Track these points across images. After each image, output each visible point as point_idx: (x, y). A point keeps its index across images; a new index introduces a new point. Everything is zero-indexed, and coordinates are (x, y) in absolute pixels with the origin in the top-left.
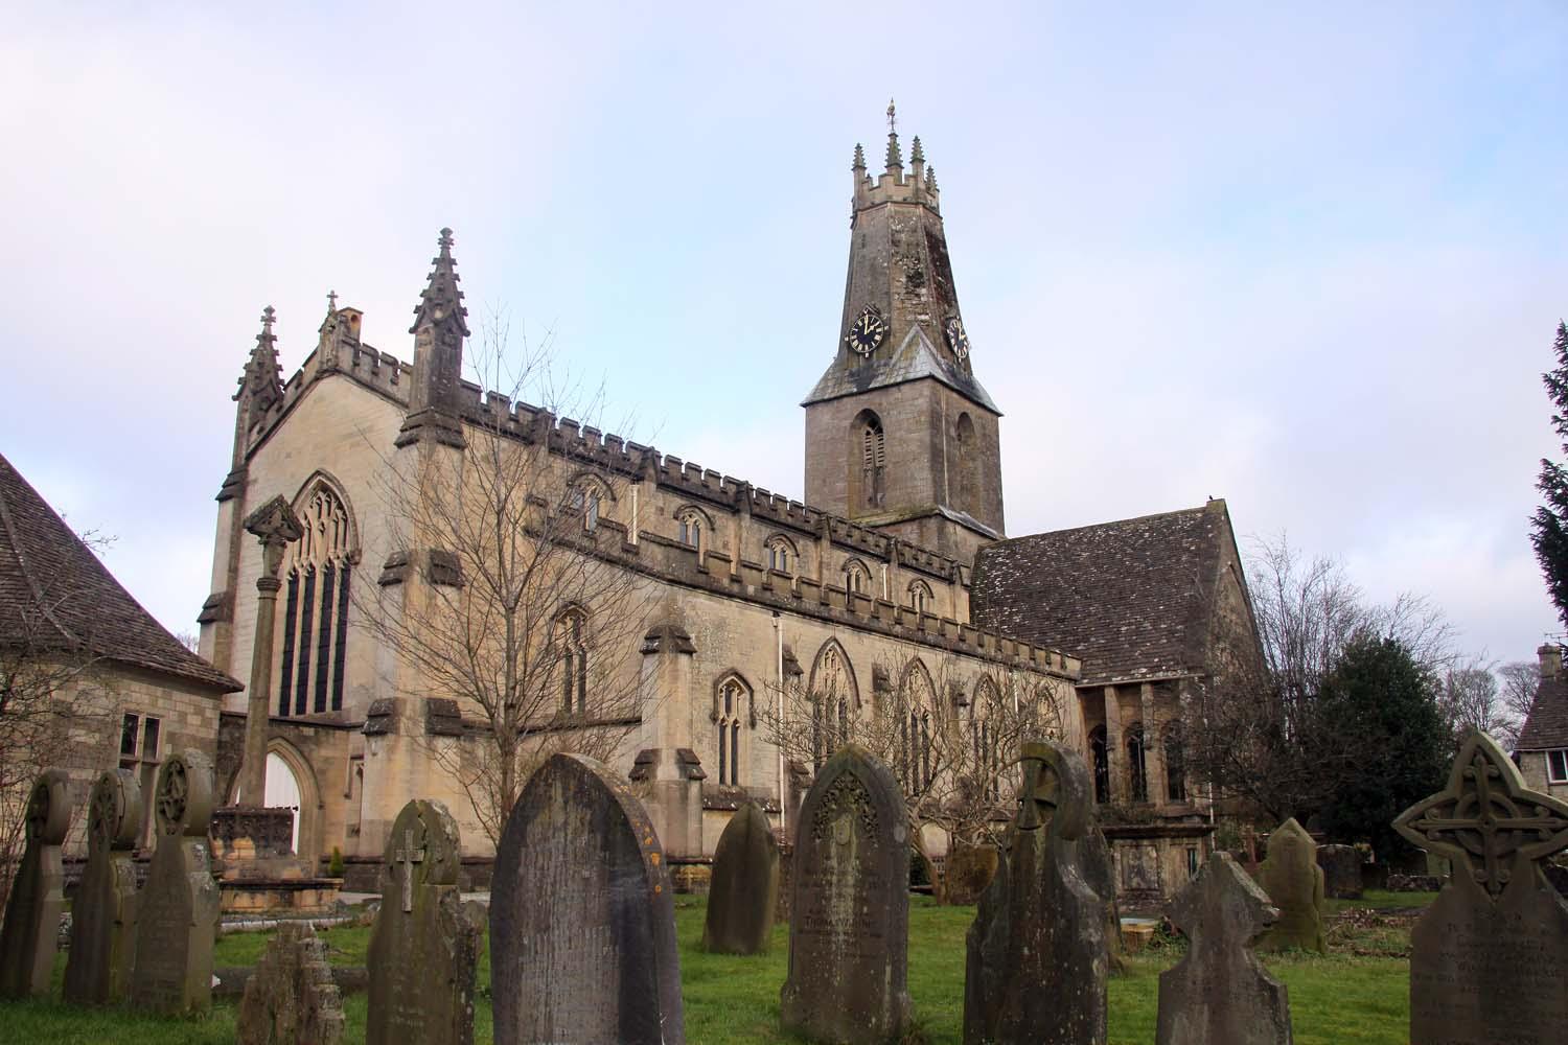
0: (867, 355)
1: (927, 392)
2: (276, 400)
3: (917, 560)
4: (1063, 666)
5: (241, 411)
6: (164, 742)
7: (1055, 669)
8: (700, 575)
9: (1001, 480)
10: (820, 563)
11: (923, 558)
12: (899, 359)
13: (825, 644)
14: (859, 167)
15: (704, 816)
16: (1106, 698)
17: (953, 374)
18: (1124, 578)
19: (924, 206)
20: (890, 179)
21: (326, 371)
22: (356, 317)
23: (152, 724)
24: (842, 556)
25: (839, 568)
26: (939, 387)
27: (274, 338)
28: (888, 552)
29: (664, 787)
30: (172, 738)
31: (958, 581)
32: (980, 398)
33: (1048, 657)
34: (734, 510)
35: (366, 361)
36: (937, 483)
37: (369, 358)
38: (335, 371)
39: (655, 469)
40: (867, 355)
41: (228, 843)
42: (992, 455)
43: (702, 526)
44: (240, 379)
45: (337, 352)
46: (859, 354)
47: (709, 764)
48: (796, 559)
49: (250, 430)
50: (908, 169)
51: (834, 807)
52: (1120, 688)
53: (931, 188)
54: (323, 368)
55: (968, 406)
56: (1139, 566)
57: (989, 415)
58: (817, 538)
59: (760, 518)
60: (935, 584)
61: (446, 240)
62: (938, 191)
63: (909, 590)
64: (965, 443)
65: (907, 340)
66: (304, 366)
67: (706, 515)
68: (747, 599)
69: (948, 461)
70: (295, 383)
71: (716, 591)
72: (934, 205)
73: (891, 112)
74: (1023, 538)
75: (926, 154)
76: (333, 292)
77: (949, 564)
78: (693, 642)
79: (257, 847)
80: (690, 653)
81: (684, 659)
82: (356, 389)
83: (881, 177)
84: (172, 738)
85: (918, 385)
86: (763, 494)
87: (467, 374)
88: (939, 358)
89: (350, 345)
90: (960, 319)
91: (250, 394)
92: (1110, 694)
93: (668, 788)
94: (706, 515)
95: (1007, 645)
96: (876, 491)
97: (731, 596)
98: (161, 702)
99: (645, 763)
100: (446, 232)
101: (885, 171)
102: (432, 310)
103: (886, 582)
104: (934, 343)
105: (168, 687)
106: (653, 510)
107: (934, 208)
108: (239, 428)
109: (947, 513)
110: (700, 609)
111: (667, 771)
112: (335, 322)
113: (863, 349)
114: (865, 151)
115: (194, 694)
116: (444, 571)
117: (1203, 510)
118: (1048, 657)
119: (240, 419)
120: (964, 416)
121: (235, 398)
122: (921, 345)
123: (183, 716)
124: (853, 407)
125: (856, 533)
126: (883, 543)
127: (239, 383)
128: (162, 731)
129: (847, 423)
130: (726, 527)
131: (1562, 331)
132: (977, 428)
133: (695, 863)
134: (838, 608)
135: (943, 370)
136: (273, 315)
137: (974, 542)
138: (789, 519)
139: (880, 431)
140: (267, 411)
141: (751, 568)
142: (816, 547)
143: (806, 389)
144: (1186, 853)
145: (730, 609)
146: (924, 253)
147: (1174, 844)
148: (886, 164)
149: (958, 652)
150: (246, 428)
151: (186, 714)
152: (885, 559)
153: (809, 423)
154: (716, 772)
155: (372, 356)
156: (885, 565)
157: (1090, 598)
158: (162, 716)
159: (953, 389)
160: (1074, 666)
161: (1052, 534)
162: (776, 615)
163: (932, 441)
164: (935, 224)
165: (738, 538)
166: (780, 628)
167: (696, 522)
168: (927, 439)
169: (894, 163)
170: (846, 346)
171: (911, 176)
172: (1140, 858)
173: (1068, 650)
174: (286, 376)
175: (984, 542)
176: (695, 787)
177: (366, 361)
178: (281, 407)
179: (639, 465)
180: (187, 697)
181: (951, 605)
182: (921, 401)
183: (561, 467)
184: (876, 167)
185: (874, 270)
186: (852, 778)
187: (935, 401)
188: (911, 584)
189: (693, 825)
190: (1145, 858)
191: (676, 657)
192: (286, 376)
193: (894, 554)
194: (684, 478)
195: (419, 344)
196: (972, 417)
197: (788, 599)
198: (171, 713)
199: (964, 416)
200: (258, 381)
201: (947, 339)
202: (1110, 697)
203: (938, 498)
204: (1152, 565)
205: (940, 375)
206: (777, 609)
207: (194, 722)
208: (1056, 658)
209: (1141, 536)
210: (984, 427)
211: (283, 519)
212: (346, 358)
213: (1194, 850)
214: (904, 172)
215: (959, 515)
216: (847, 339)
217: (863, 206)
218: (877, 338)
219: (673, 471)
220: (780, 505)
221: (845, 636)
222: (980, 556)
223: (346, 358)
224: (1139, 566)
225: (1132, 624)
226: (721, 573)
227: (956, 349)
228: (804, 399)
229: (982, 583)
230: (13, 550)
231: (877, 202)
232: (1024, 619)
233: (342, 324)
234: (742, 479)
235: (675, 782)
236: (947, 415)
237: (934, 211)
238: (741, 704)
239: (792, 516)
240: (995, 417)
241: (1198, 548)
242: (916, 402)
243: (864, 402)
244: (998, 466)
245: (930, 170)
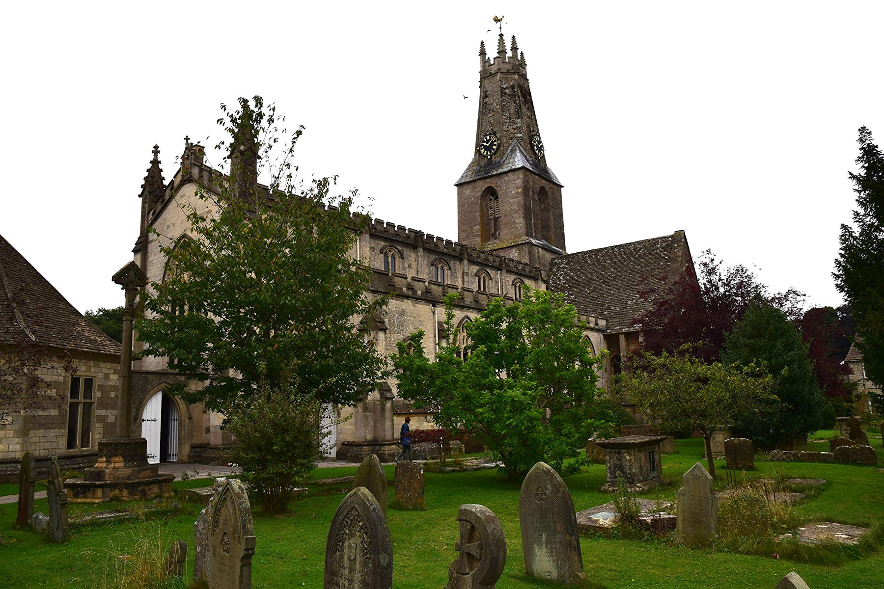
0: (489, 157)
1: (521, 176)
2: (161, 196)
3: (517, 268)
4: (597, 324)
5: (144, 203)
6: (96, 390)
7: (592, 325)
8: (389, 287)
9: (563, 222)
11: (520, 267)
12: (506, 159)
13: (462, 320)
14: (483, 53)
15: (395, 418)
16: (620, 340)
17: (534, 165)
18: (630, 274)
19: (518, 73)
20: (500, 60)
21: (185, 180)
23: (89, 382)
24: (475, 269)
25: (473, 275)
26: (528, 173)
27: (160, 162)
28: (500, 265)
29: (372, 404)
30: (101, 388)
31: (540, 278)
32: (551, 178)
33: (587, 319)
34: (414, 247)
35: (205, 174)
37: (207, 173)
39: (369, 227)
40: (489, 157)
41: (109, 459)
42: (558, 209)
43: (397, 256)
44: (142, 185)
45: (191, 170)
46: (485, 156)
48: (449, 271)
49: (149, 213)
50: (509, 54)
51: (347, 531)
52: (627, 334)
53: (522, 64)
54: (185, 177)
56: (637, 268)
57: (556, 187)
58: (461, 260)
59: (427, 250)
60: (527, 280)
61: (156, 151)
62: (526, 65)
63: (513, 284)
64: (543, 203)
65: (510, 148)
66: (174, 177)
67: (399, 250)
69: (534, 214)
70: (170, 187)
72: (524, 73)
73: (299, 133)
74: (575, 254)
76: (187, 137)
77: (535, 269)
78: (387, 324)
79: (125, 461)
80: (384, 330)
83: (495, 59)
84: (101, 388)
85: (517, 173)
86: (430, 237)
88: (528, 157)
89: (198, 166)
90: (539, 136)
91: (147, 194)
93: (374, 404)
94: (399, 250)
96: (496, 231)
98: (93, 369)
101: (497, 55)
102: (239, 145)
104: (526, 150)
105: (97, 361)
106: (368, 249)
107: (524, 74)
108: (143, 212)
109: (533, 241)
112: (189, 153)
113: (487, 154)
114: (517, 39)
115: (109, 362)
117: (672, 236)
118: (587, 319)
119: (143, 208)
120: (542, 188)
121: (140, 196)
122: (518, 151)
123: (107, 376)
124: (482, 186)
125: (482, 256)
126: (498, 260)
127: (142, 187)
128: (95, 385)
129: (479, 194)
130: (410, 256)
131: (869, 152)
132: (549, 194)
133: (390, 445)
135: (530, 164)
136: (158, 150)
137: (548, 256)
138: (445, 250)
139: (497, 198)
140: (156, 203)
141: (419, 281)
142: (460, 264)
143: (457, 177)
144: (648, 454)
145: (407, 305)
147: (641, 451)
148: (498, 51)
150: (147, 212)
151: (109, 374)
152: (499, 269)
155: (209, 172)
156: (499, 272)
157: (611, 286)
158: (94, 377)
159: (535, 174)
160: (602, 323)
161: (590, 251)
162: (434, 306)
163: (524, 202)
164: (525, 84)
166: (436, 312)
167: (393, 254)
168: (522, 202)
169: (502, 52)
170: (478, 152)
171: (511, 58)
172: (620, 460)
174: (166, 183)
175: (553, 256)
176: (388, 404)
177: (205, 174)
178: (163, 201)
180: (109, 365)
182: (518, 181)
184: (492, 53)
186: (357, 513)
187: (526, 181)
188: (513, 281)
189: (388, 424)
190: (624, 460)
191: (377, 333)
192: (166, 183)
193: (504, 265)
194: (385, 230)
196: (547, 189)
197: (440, 296)
198: (99, 374)
199: (542, 188)
200: (151, 186)
201: (532, 146)
204: (644, 267)
205: (528, 166)
207: (114, 378)
208: (592, 319)
209: (639, 251)
210: (553, 194)
211: (135, 275)
212: (195, 171)
213: (653, 452)
214: (508, 55)
215: (540, 242)
216: (478, 148)
217: (486, 75)
218: (494, 147)
219: (379, 227)
220: (439, 243)
222: (552, 264)
224: (637, 268)
225: (633, 299)
227: (537, 152)
228: (455, 182)
229: (553, 278)
230: (4, 289)
231: (493, 72)
232: (576, 297)
234: (418, 230)
235: (378, 401)
236: (533, 188)
237: (524, 77)
239: (446, 248)
240: (559, 188)
241: (670, 257)
242: (516, 182)
244: (561, 214)
245: (522, 53)
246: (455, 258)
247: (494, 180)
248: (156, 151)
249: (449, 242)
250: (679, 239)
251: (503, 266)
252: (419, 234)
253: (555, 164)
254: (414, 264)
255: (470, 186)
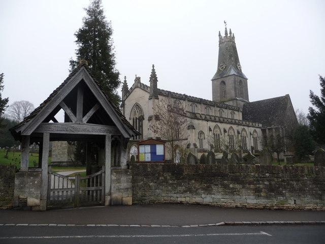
10: (215, 112)
14: (220, 35)
17: (238, 73)
22: (140, 78)
24: (219, 109)
34: (200, 103)
36: (236, 94)
38: (138, 87)
47: (198, 145)
50: (229, 35)
53: (234, 37)
55: (241, 79)
61: (153, 66)
68: (203, 120)
71: (198, 119)
75: (232, 32)
80: (194, 129)
81: (194, 130)
82: (141, 90)
87: (158, 87)
92: (267, 130)
95: (247, 123)
97: (200, 120)
99: (189, 146)
100: (153, 65)
103: (227, 114)
110: (196, 122)
111: (192, 147)
116: (157, 118)
120: (241, 81)
124: (220, 80)
134: (217, 119)
146: (232, 50)
149: (238, 125)
152: (226, 108)
153: (213, 83)
154: (62, 144)
160: (260, 125)
165: (200, 110)
169: (226, 34)
173: (260, 122)
179: (185, 98)
181: (238, 116)
183: (173, 100)
184: (223, 35)
185: (224, 55)
187: (235, 78)
195: (151, 83)
199: (241, 81)
202: (267, 131)
203: (236, 96)
205: (236, 74)
206: (207, 121)
217: (221, 43)
221: (219, 124)
222: (244, 105)
223: (139, 85)
226: (198, 116)
233: (138, 80)
237: (234, 42)
238: (203, 136)
243: (222, 79)
246: (212, 106)
247: (225, 78)
248: (153, 66)
249: (210, 101)
250: (286, 99)
251: (227, 107)
252: (201, 99)
253: (245, 71)
254: (200, 109)
255: (217, 80)
